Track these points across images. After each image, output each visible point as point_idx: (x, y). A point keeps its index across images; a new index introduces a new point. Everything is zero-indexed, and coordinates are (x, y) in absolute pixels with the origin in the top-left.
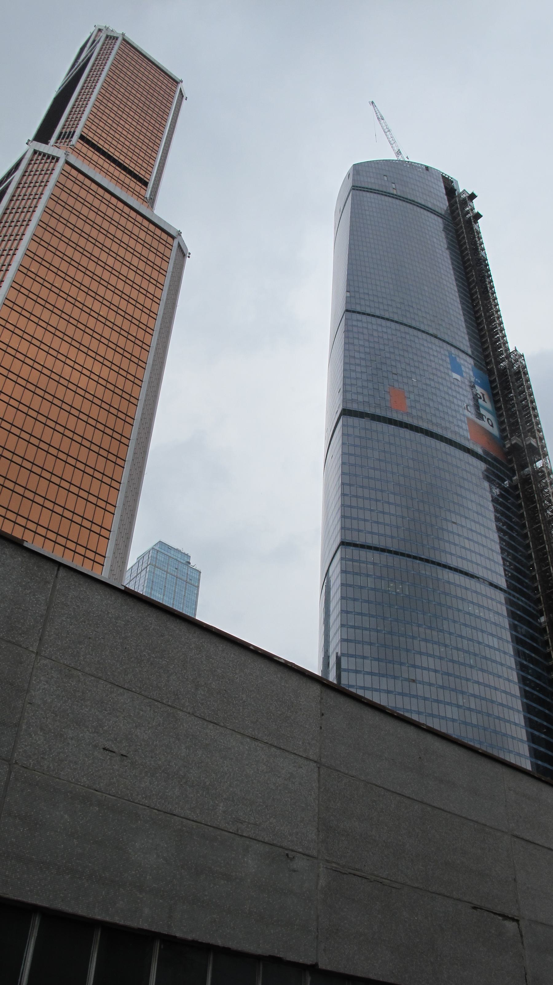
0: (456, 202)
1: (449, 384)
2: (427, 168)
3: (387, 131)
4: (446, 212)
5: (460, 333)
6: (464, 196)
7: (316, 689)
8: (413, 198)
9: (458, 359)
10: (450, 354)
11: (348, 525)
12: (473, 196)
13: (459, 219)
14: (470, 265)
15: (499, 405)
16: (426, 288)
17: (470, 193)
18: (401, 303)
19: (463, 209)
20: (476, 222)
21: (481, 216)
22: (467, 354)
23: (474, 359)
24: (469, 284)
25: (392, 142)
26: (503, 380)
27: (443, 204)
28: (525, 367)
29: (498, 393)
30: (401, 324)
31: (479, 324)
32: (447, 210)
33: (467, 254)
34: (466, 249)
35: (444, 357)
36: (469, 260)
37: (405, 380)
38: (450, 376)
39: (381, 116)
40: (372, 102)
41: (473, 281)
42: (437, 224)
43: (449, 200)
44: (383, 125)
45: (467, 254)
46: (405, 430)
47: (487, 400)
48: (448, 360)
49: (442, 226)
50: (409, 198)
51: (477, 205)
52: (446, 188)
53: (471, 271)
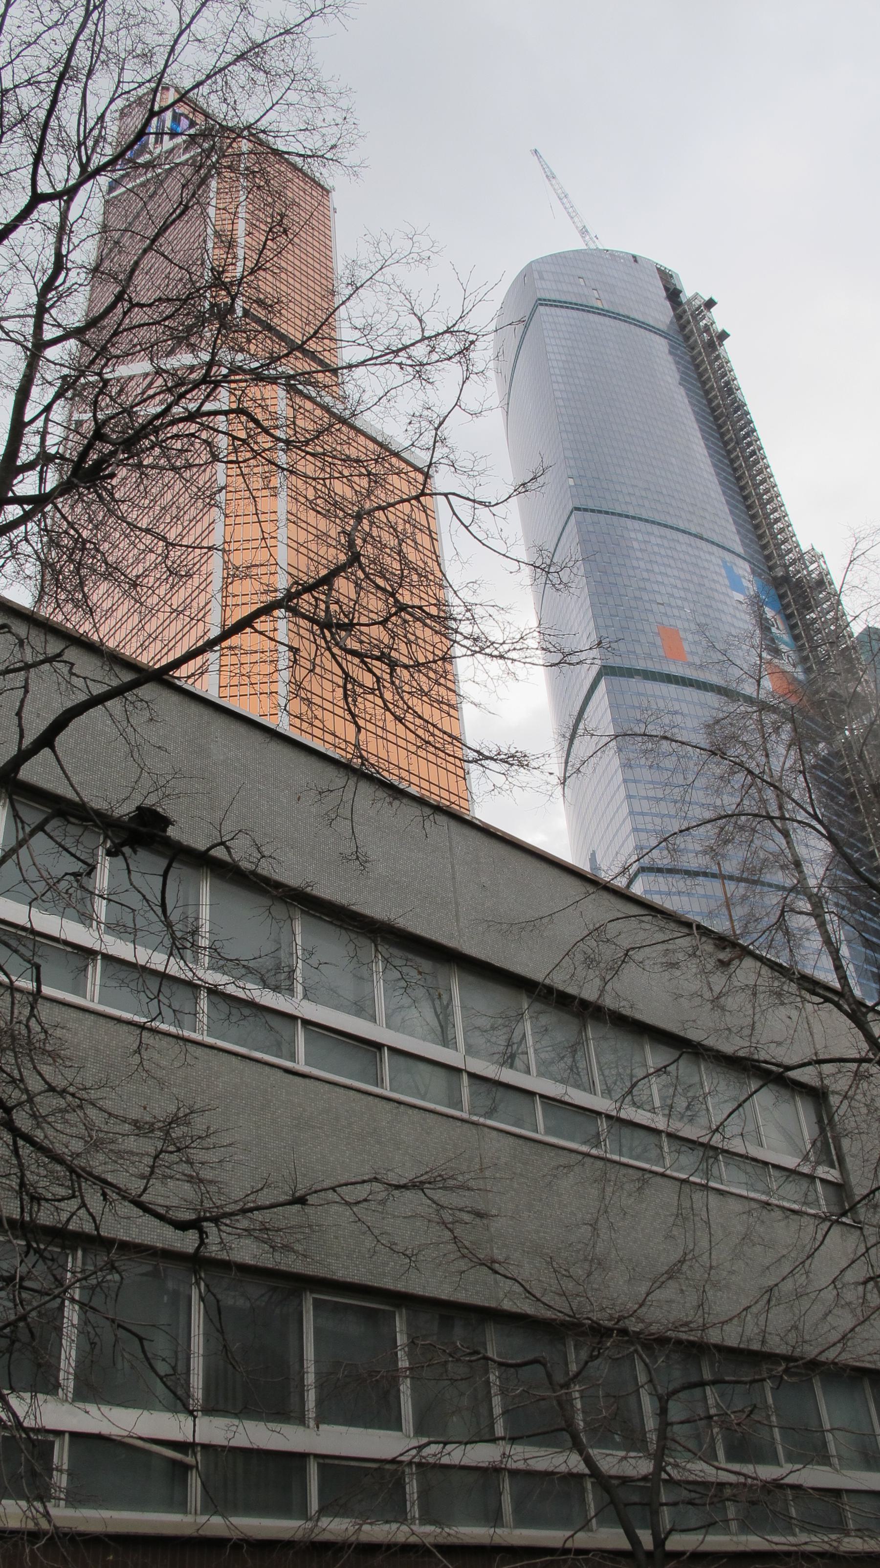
0: (685, 311)
1: (732, 611)
2: (635, 259)
3: (563, 197)
4: (669, 327)
5: (724, 524)
6: (697, 303)
7: (575, 888)
8: (626, 313)
9: (735, 568)
10: (724, 562)
11: (637, 809)
12: (710, 304)
13: (694, 339)
14: (722, 414)
15: (797, 632)
16: (673, 460)
17: (707, 299)
18: (645, 489)
19: (697, 323)
20: (721, 345)
21: (728, 335)
22: (739, 556)
23: (749, 562)
24: (726, 444)
25: (573, 214)
26: (794, 593)
27: (662, 314)
28: (828, 573)
29: (793, 613)
30: (653, 522)
31: (749, 507)
32: (671, 322)
33: (716, 397)
34: (712, 388)
35: (717, 569)
36: (718, 406)
37: (676, 612)
38: (731, 598)
39: (552, 173)
40: (536, 151)
41: (731, 439)
42: (661, 345)
43: (674, 309)
44: (556, 187)
45: (716, 397)
46: (691, 689)
47: (781, 627)
48: (723, 572)
49: (677, 376)
50: (621, 312)
51: (719, 318)
52: (667, 289)
53: (725, 423)
